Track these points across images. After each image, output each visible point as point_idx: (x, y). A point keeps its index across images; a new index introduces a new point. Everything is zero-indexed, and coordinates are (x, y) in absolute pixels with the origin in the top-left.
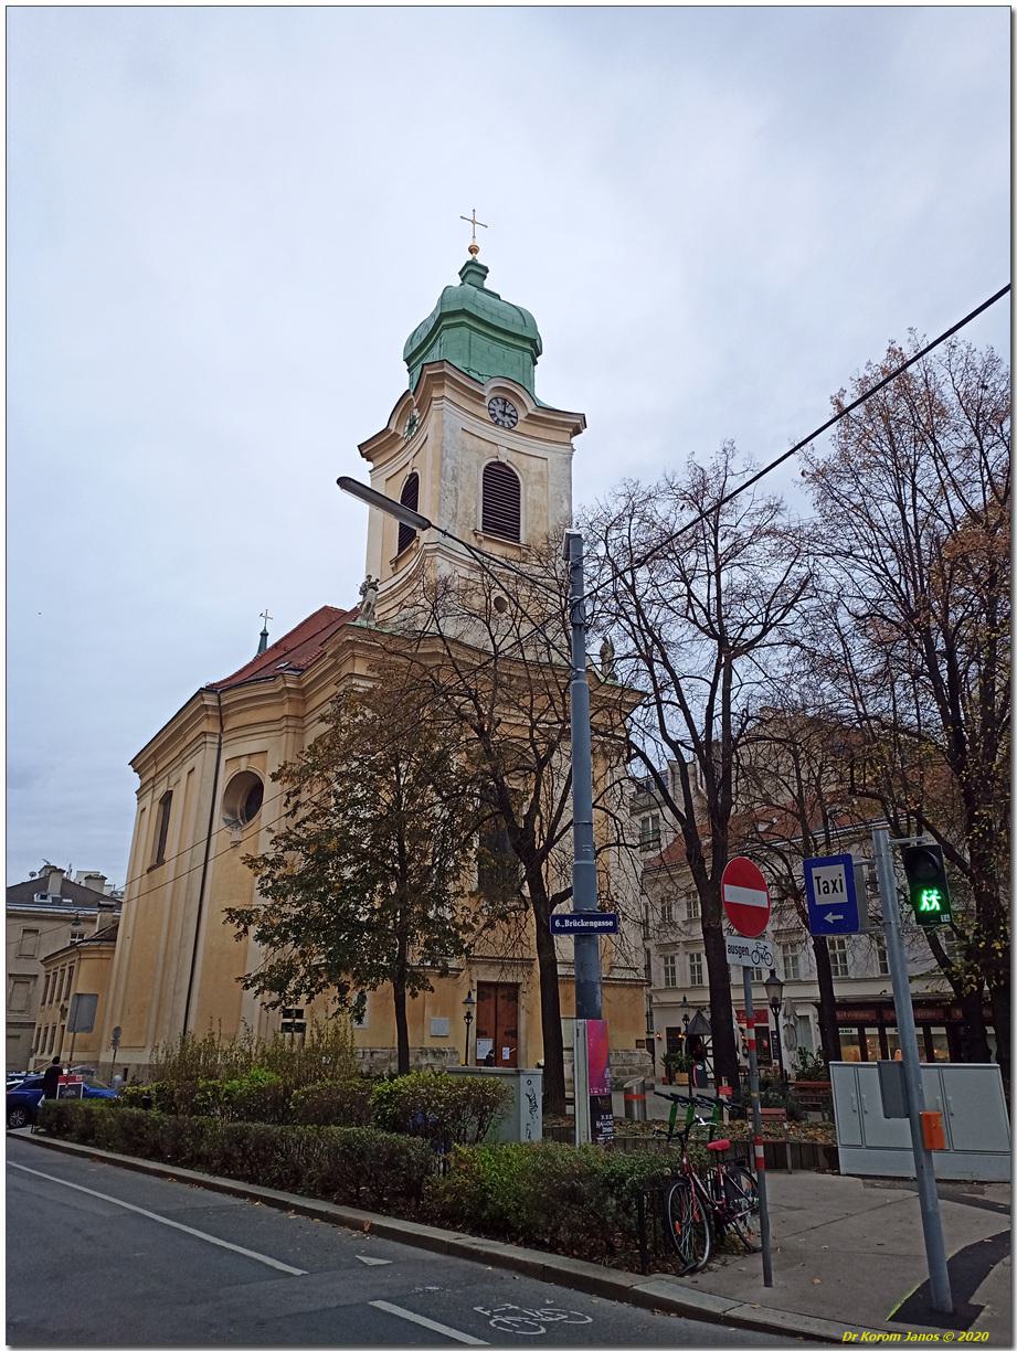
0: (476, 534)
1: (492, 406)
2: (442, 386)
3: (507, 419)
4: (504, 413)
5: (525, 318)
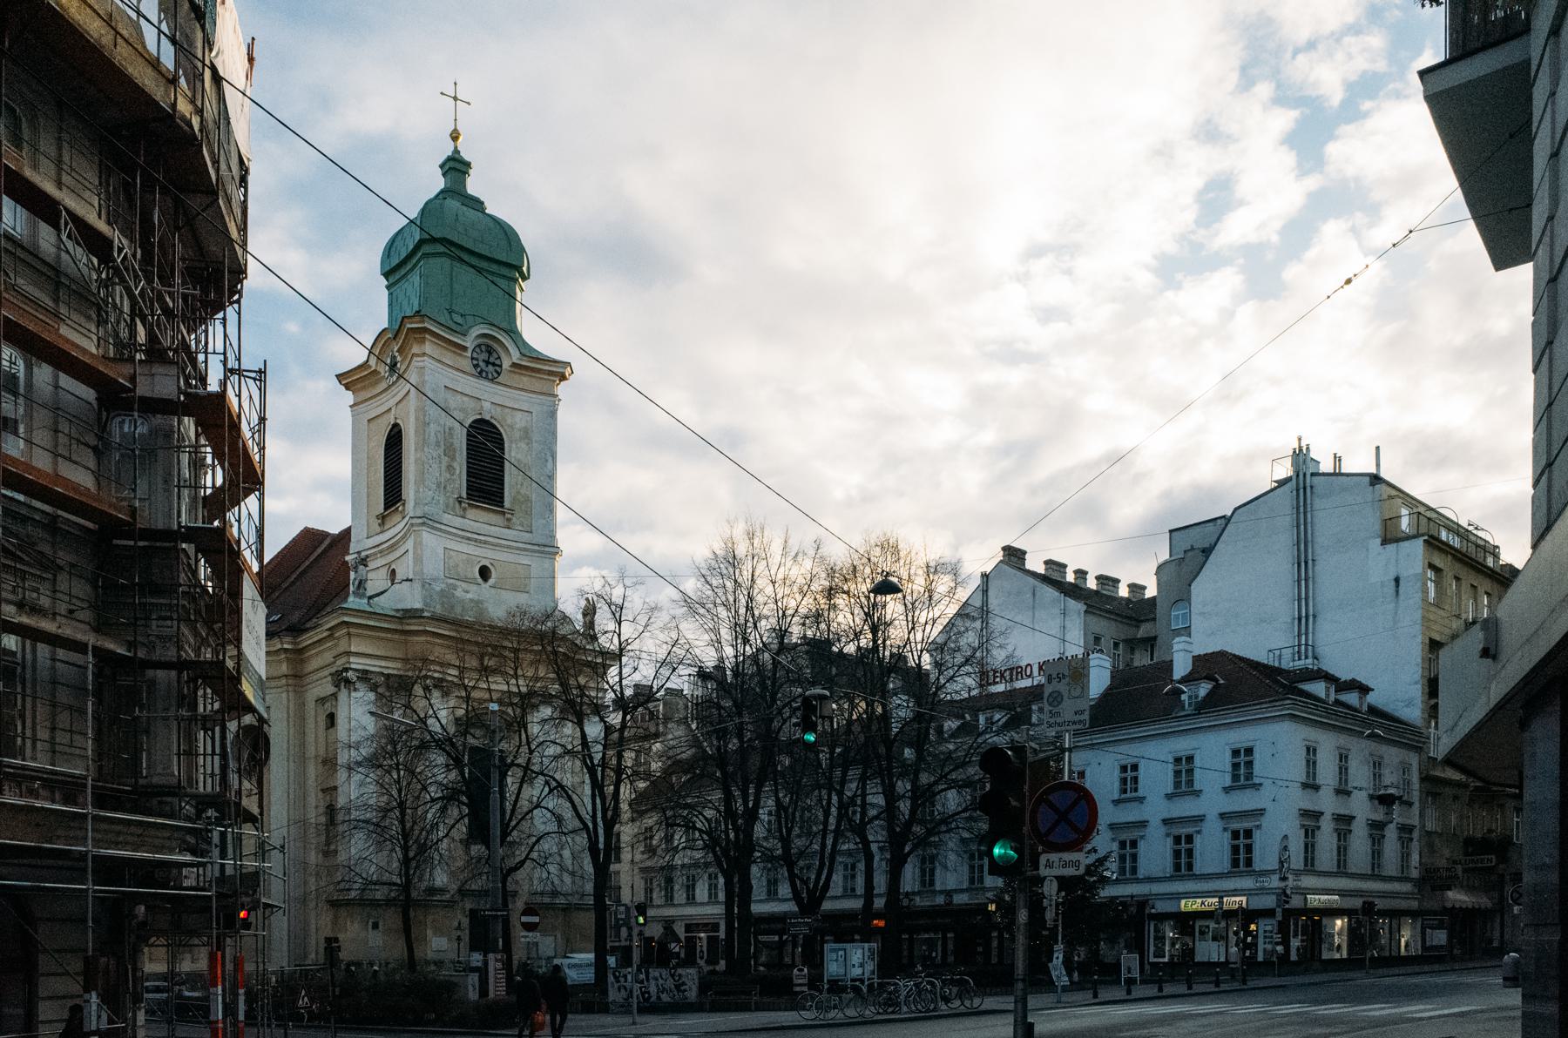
0: (460, 502)
1: (475, 355)
2: (423, 341)
3: (491, 368)
4: (487, 363)
5: (508, 235)
